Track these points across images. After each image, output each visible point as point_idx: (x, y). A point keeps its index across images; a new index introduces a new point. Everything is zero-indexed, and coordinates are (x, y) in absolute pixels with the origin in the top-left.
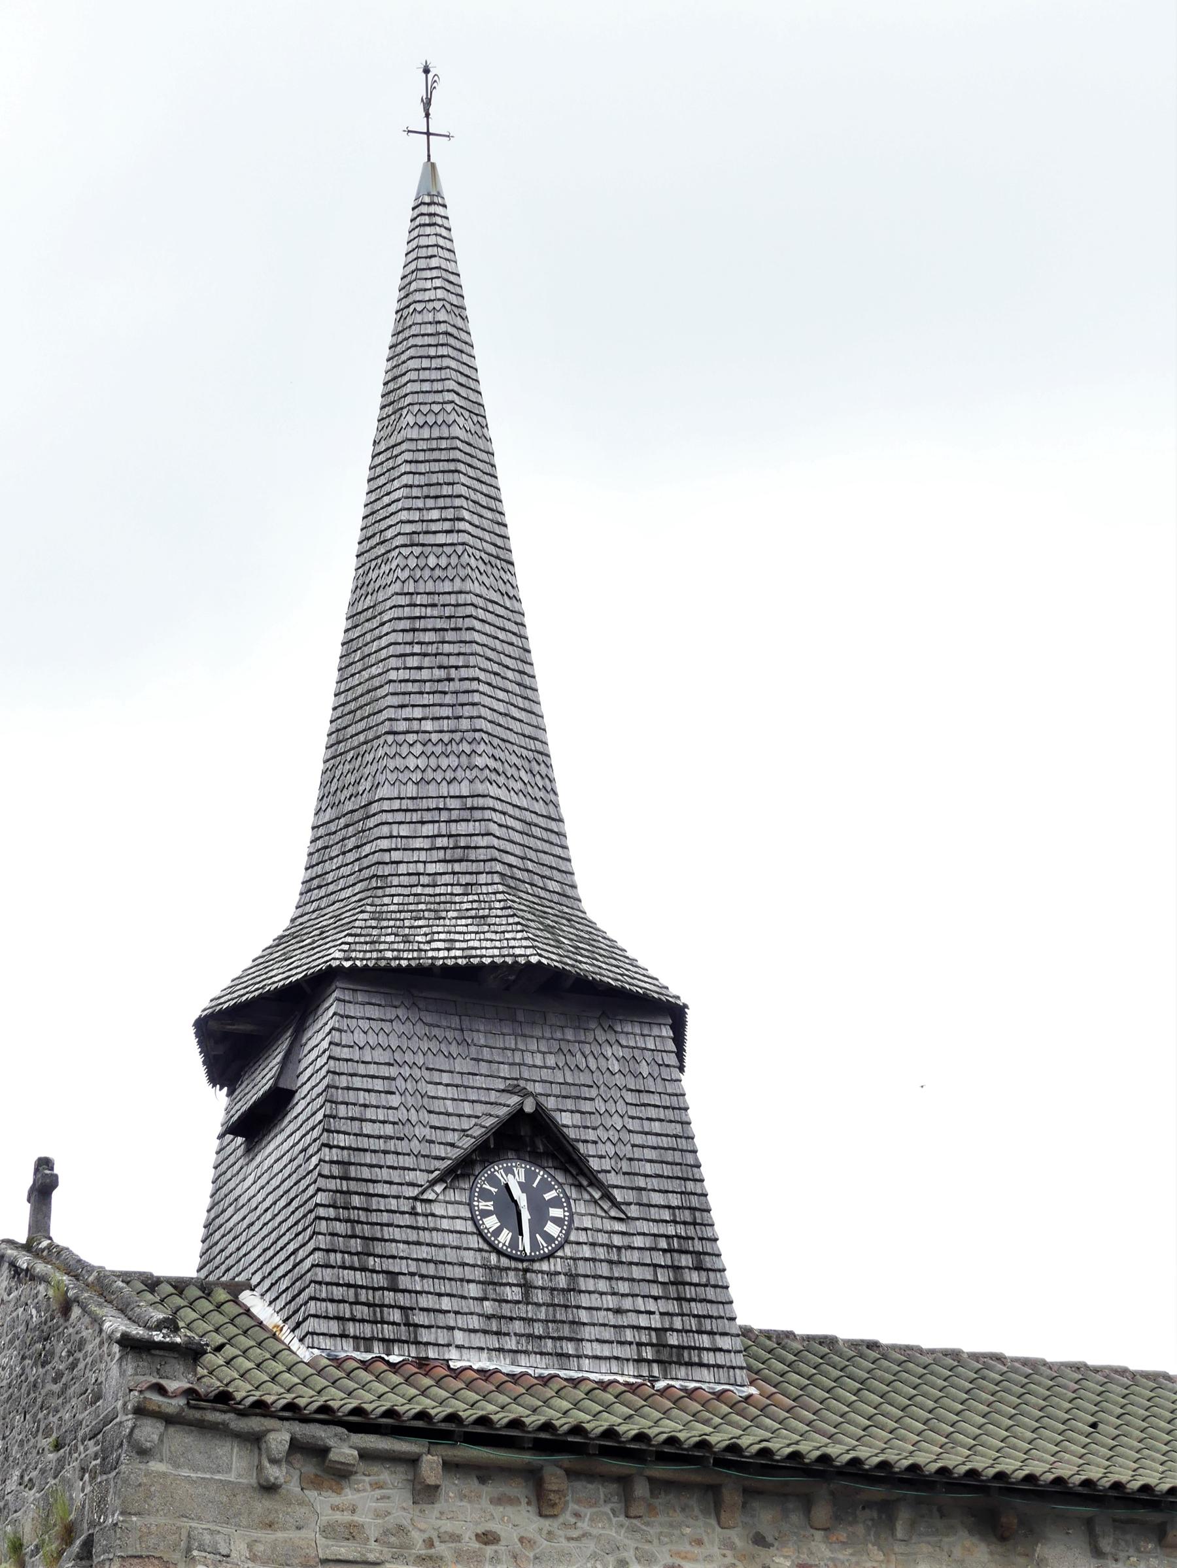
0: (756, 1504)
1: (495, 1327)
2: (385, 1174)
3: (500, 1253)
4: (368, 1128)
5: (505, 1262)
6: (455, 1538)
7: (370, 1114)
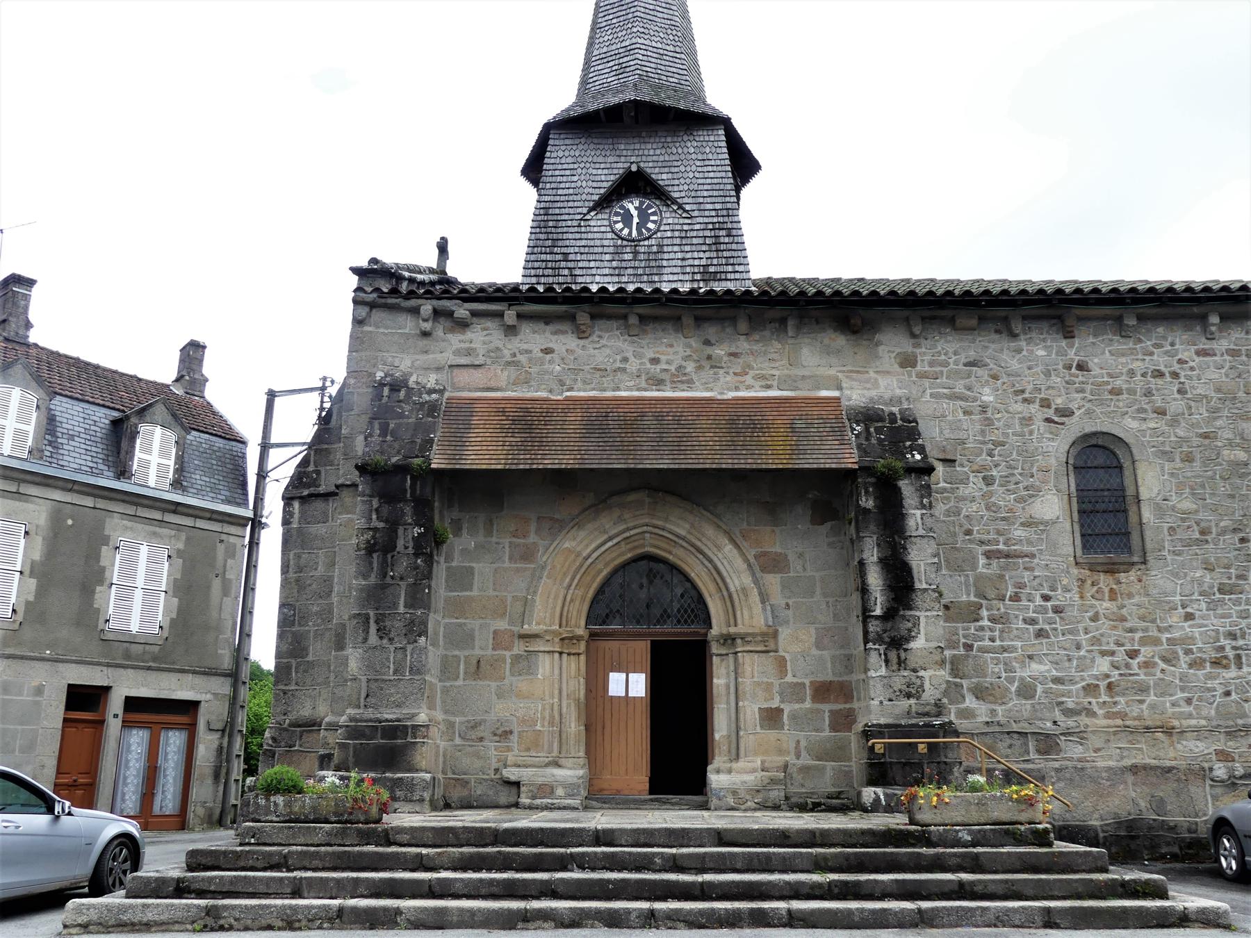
0: (706, 325)
2: (567, 211)
3: (623, 239)
4: (560, 192)
5: (625, 243)
6: (528, 352)
7: (562, 185)
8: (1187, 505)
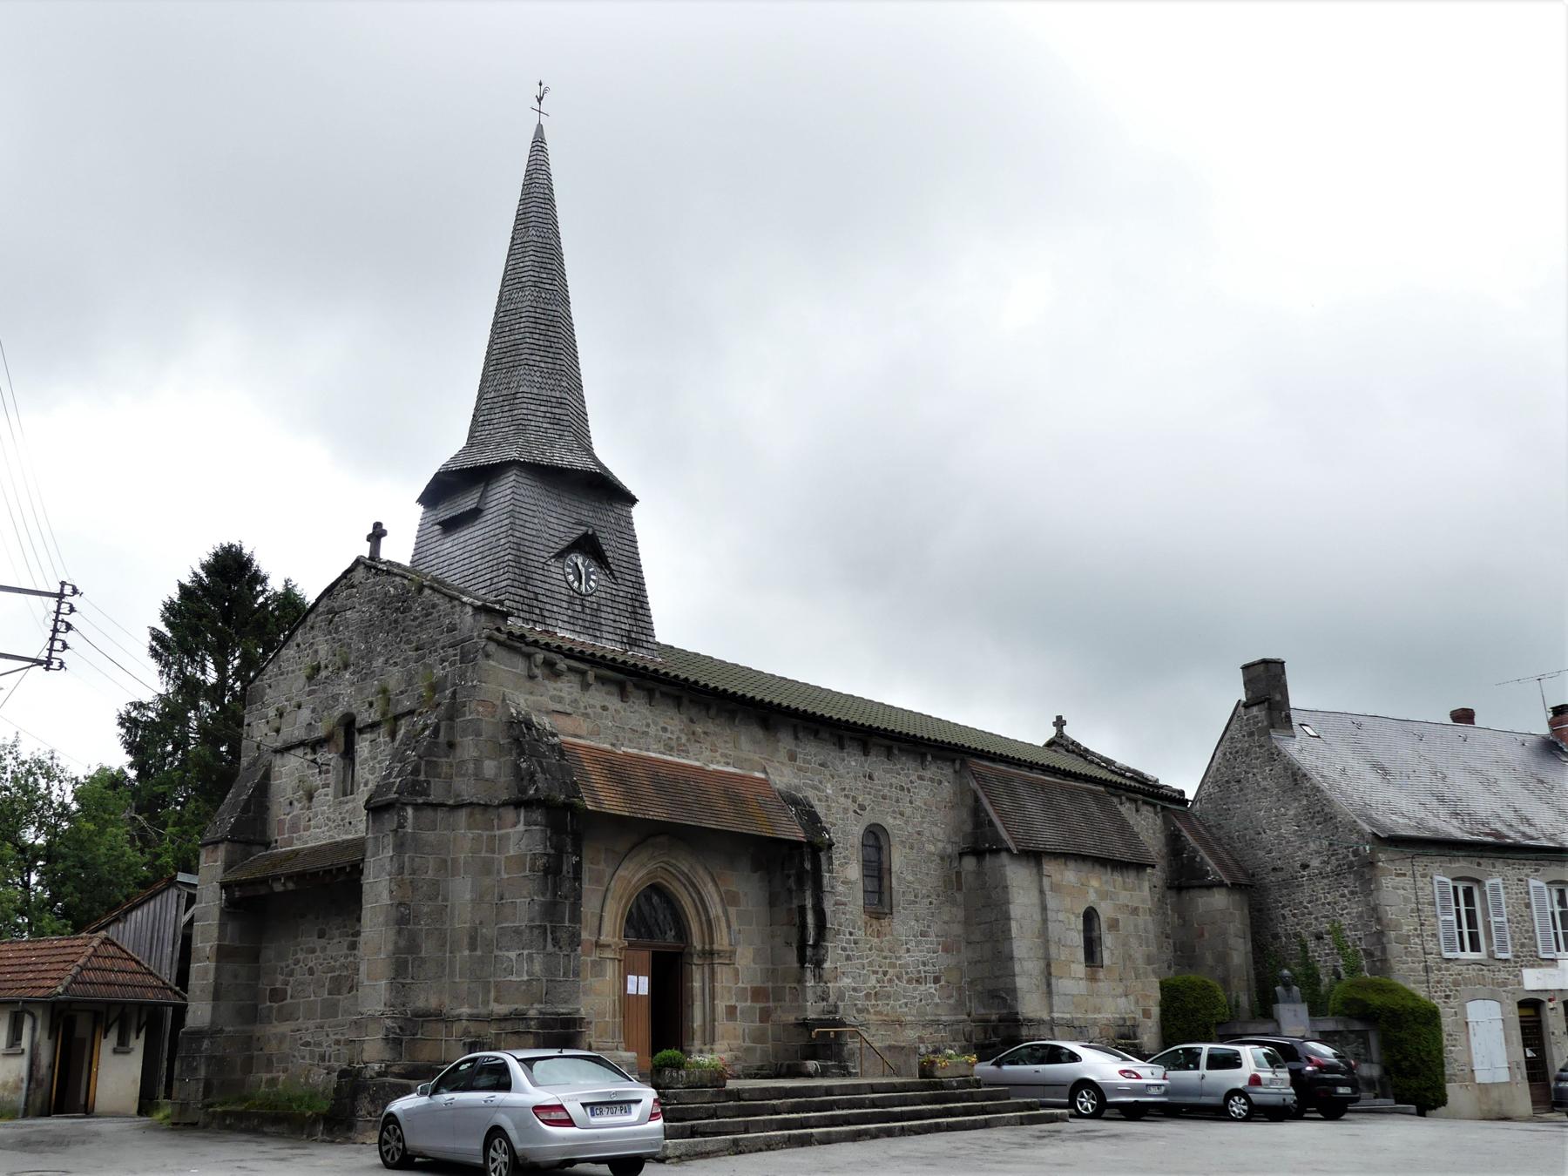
1: (572, 621)
8: (910, 878)
